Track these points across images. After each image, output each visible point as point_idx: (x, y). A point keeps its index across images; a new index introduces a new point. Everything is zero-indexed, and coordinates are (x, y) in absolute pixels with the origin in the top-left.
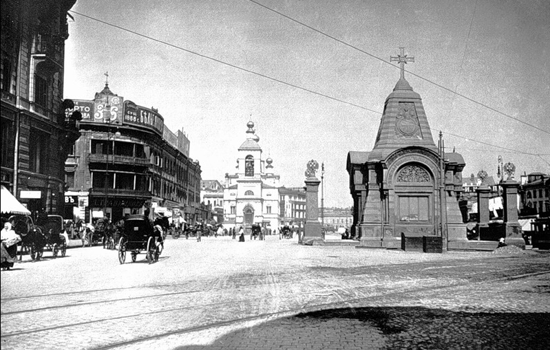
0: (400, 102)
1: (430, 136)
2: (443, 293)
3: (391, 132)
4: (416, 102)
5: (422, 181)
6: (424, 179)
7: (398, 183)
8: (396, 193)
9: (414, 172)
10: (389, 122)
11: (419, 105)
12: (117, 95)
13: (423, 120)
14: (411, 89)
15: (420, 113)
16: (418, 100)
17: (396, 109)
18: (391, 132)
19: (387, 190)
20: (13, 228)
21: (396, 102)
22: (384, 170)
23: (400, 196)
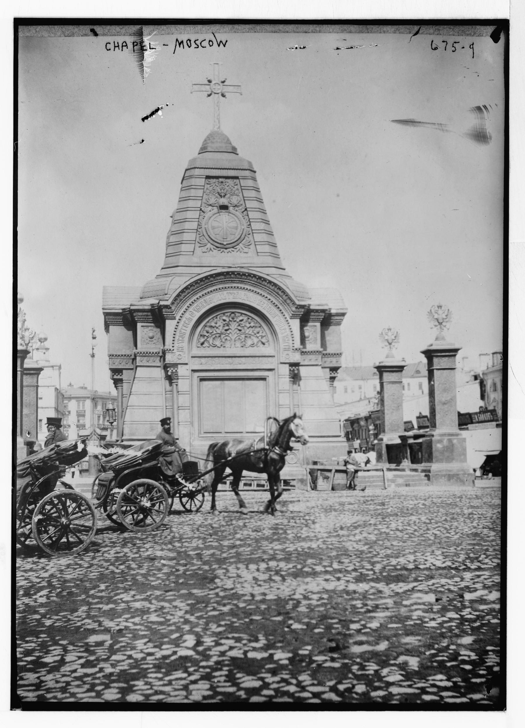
0: (208, 177)
1: (272, 249)
2: (374, 481)
3: (188, 242)
4: (245, 178)
5: (252, 345)
6: (255, 340)
7: (196, 352)
8: (194, 371)
9: (234, 326)
10: (184, 221)
11: (250, 183)
12: (165, 422)
13: (262, 226)
14: (234, 151)
15: (248, 189)
16: (247, 173)
17: (200, 193)
18: (188, 242)
19: (175, 365)
20: (493, 475)
21: (199, 177)
22: (168, 322)
23: (202, 380)
